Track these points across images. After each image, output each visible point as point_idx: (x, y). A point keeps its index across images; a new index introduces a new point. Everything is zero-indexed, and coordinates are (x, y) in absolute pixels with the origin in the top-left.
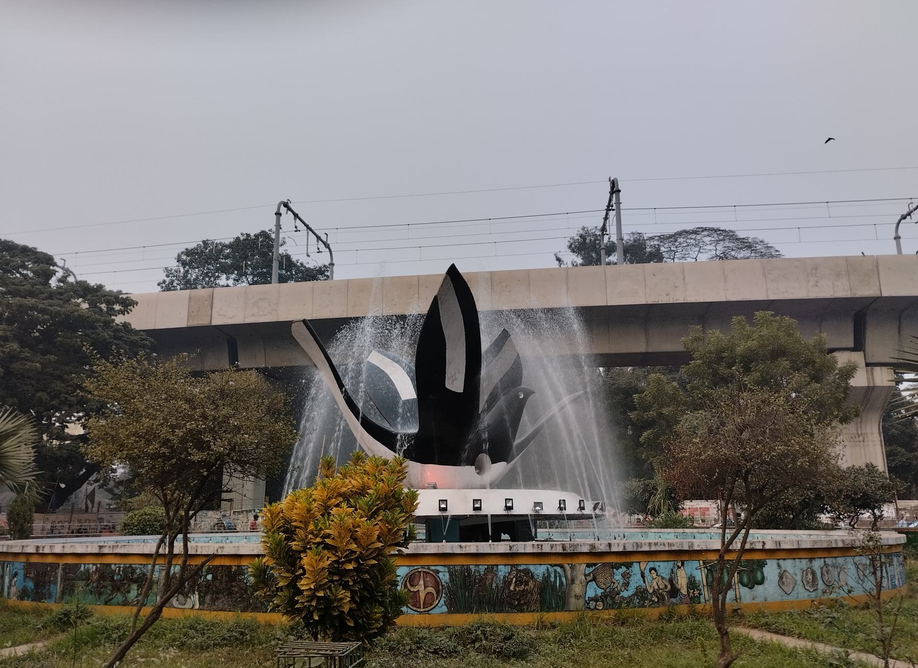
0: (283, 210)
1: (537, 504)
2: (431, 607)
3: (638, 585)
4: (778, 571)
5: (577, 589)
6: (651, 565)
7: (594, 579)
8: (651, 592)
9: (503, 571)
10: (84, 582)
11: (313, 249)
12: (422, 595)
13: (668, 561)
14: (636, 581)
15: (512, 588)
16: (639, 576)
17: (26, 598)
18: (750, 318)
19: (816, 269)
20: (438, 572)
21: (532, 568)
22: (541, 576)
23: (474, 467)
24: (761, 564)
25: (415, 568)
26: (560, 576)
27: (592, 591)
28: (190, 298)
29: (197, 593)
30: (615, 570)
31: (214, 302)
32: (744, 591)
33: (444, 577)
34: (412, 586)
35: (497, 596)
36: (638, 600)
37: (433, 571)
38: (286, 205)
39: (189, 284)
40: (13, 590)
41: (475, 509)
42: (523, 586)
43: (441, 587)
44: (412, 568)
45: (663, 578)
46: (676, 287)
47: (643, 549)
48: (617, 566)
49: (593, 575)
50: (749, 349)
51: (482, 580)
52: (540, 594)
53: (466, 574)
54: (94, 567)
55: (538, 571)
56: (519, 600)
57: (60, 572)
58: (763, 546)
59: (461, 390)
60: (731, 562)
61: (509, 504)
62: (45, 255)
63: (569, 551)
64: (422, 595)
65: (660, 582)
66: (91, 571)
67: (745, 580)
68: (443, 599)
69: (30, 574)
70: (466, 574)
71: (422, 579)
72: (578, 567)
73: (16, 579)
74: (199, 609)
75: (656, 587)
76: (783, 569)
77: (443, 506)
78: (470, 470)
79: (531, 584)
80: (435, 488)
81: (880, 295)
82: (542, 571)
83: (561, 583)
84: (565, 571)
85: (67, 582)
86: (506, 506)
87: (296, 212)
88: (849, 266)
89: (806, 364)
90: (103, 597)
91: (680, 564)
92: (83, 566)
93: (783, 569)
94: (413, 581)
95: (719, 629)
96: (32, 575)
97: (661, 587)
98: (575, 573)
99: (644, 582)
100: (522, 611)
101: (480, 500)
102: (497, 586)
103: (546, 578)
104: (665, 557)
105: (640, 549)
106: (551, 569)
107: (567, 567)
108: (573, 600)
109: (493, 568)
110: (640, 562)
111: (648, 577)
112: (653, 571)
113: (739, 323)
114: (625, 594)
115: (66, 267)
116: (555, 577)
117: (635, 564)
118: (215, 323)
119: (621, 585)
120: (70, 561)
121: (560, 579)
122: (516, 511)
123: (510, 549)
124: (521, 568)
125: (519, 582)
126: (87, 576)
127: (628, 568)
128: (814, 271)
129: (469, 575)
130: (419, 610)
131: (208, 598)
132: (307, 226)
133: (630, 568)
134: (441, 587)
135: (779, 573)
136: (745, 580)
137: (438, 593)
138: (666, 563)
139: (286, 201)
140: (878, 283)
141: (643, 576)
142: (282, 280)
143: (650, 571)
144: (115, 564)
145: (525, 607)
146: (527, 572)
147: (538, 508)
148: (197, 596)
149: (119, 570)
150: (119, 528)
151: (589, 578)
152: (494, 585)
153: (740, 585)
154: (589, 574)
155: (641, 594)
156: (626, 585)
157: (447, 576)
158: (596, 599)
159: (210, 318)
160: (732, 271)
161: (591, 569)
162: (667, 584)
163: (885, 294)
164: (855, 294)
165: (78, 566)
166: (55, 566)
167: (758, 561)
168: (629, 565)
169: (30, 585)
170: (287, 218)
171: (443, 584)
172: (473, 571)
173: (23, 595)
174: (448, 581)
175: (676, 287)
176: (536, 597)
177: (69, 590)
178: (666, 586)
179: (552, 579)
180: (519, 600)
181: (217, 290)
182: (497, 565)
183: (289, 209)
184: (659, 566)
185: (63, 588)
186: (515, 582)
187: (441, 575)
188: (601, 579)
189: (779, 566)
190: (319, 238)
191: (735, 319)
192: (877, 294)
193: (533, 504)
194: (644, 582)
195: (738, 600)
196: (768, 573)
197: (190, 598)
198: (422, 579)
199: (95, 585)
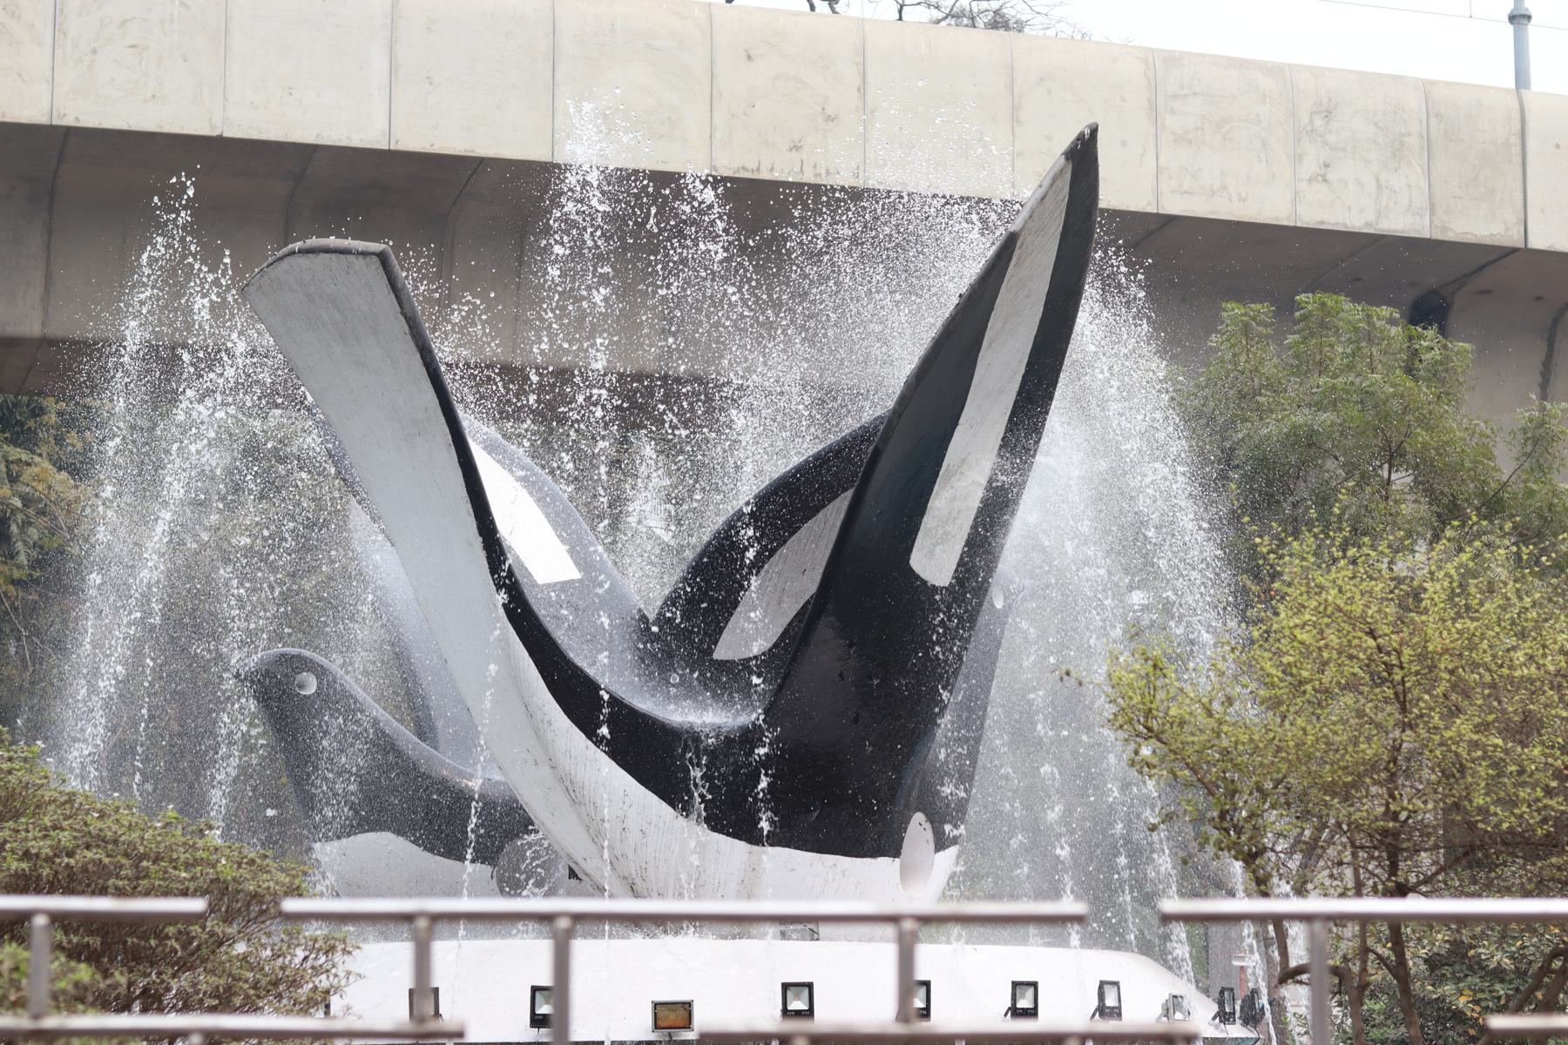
19: (1328, 115)
46: (830, 119)
77: (1024, 1003)
81: (1521, 245)
88: (1433, 121)
122: (1049, 1020)
128: (1319, 123)
140: (1520, 196)
150: (90, 999)
163: (1536, 242)
164: (1445, 229)
175: (830, 119)
191: (1233, 310)
192: (1512, 238)
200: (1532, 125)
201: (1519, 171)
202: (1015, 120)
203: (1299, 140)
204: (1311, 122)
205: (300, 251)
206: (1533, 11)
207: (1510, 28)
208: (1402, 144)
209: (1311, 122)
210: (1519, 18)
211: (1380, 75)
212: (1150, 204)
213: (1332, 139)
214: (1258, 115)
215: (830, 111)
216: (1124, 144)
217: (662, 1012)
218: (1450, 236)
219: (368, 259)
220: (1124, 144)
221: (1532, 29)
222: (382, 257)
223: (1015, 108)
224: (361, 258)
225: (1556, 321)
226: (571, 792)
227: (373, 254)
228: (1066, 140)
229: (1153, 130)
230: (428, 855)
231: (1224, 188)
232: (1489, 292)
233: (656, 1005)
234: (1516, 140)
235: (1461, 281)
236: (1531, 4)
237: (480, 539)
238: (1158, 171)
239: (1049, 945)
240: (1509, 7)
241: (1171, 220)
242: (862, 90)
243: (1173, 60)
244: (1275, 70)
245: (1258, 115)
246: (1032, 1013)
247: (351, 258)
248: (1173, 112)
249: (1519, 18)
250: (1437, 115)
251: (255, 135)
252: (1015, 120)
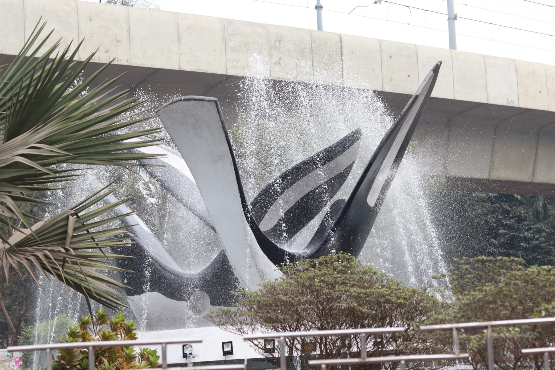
19: (280, 41)
77: (227, 349)
88: (313, 44)
128: (277, 44)
164: (143, 64)
175: (118, 41)
203: (271, 50)
204: (275, 44)
205: (184, 100)
206: (323, 5)
207: (315, 11)
208: (304, 52)
209: (275, 44)
210: (318, 8)
211: (296, 28)
212: (224, 71)
214: (258, 41)
215: (118, 39)
216: (215, 51)
219: (211, 103)
220: (215, 51)
221: (323, 11)
222: (215, 102)
223: (179, 39)
224: (208, 103)
226: (262, 276)
227: (213, 101)
229: (224, 46)
230: (168, 299)
234: (339, 50)
236: (322, 3)
237: (239, 194)
239: (198, 327)
240: (315, 4)
242: (129, 31)
243: (230, 22)
244: (263, 26)
245: (258, 41)
246: (231, 353)
247: (204, 102)
248: (231, 40)
249: (318, 8)
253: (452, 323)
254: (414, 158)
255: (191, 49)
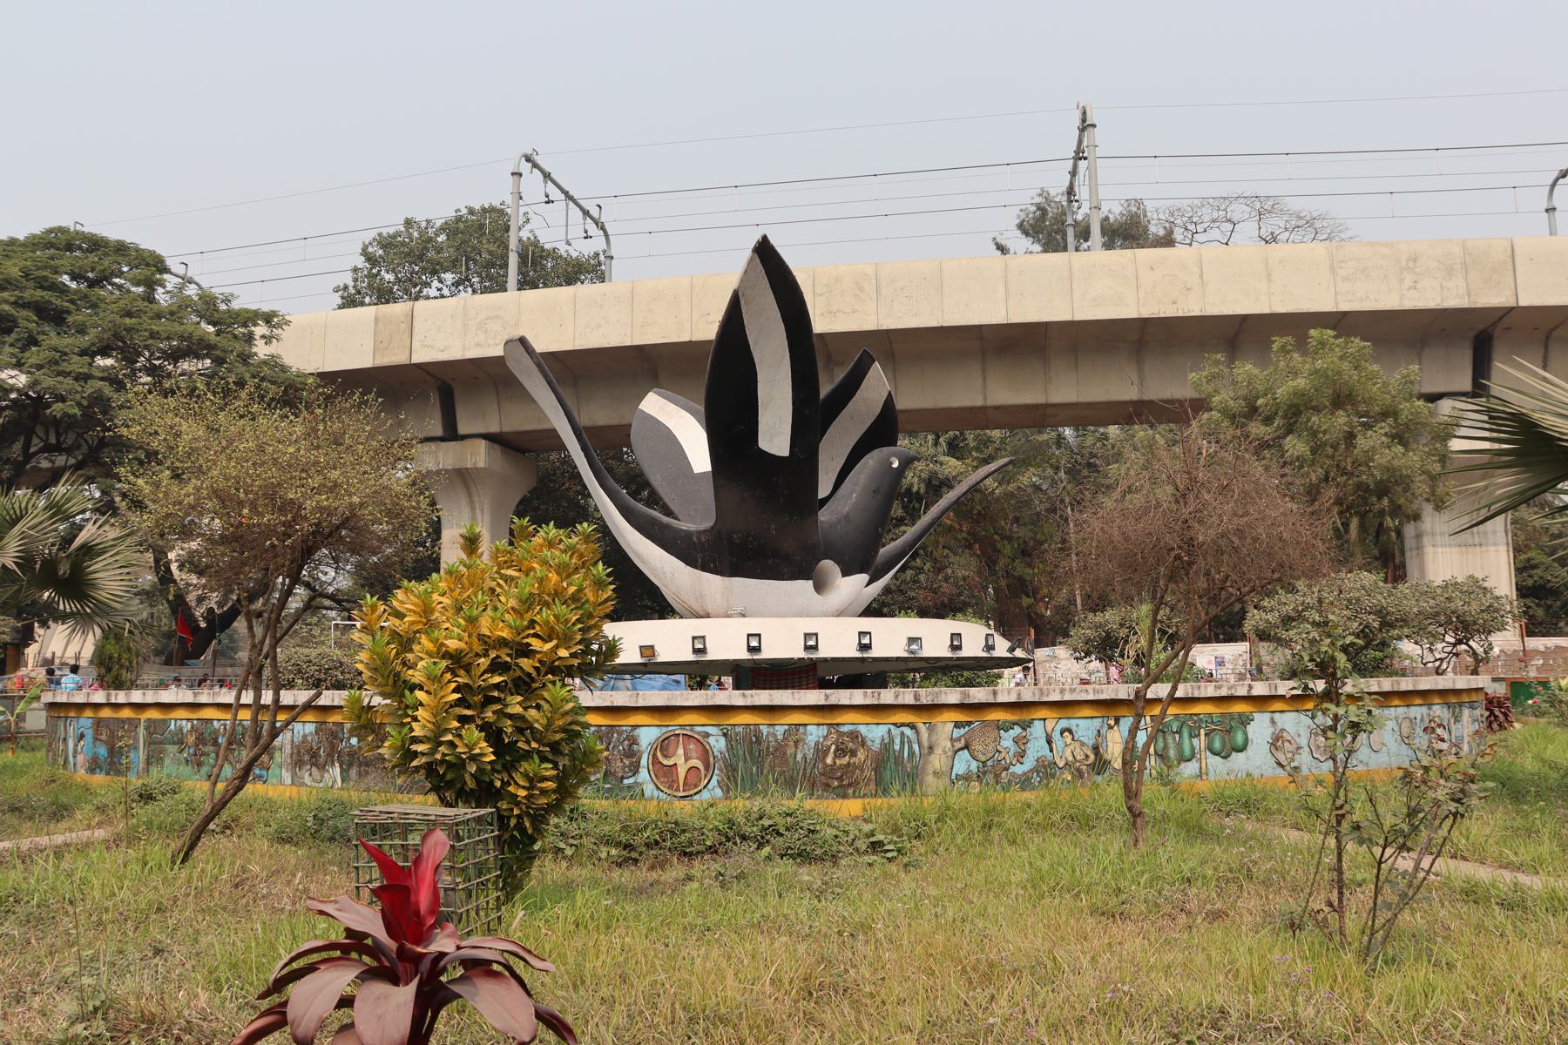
0: (525, 167)
1: (912, 640)
2: (696, 790)
3: (1039, 755)
4: (1272, 730)
5: (937, 761)
6: (1064, 723)
7: (967, 747)
8: (1061, 765)
9: (815, 733)
10: (176, 747)
11: (576, 232)
12: (682, 771)
13: (1092, 718)
14: (1037, 748)
15: (829, 761)
16: (1043, 742)
17: (98, 770)
18: (1302, 344)
19: (1415, 260)
20: (707, 735)
21: (863, 729)
22: (878, 741)
23: (811, 582)
24: (1245, 721)
25: (670, 728)
26: (910, 742)
27: (963, 763)
28: (377, 319)
29: (337, 765)
30: (1002, 732)
31: (415, 324)
32: (1214, 762)
33: (718, 744)
34: (666, 756)
35: (804, 774)
36: (1038, 779)
37: (698, 733)
38: (528, 159)
39: (385, 296)
40: (80, 758)
41: (807, 648)
42: (847, 757)
43: (711, 759)
44: (665, 729)
45: (1083, 744)
47: (1051, 699)
48: (1007, 727)
49: (966, 741)
50: (1297, 393)
51: (780, 748)
52: (876, 770)
53: (754, 739)
54: (189, 724)
55: (874, 734)
56: (840, 779)
57: (142, 732)
58: (1249, 691)
59: (787, 455)
60: (1195, 718)
61: (866, 641)
62: (152, 254)
63: (925, 702)
64: (682, 771)
65: (1078, 750)
66: (185, 731)
67: (1217, 745)
68: (715, 778)
69: (101, 734)
70: (754, 739)
71: (681, 746)
72: (940, 727)
73: (82, 743)
74: (342, 789)
75: (1070, 758)
76: (1280, 726)
77: (754, 643)
78: (807, 586)
79: (861, 755)
80: (744, 616)
82: (880, 734)
83: (911, 753)
84: (917, 733)
85: (153, 747)
86: (860, 643)
87: (548, 169)
88: (1467, 256)
89: (1384, 415)
90: (205, 770)
91: (1112, 722)
92: (173, 722)
93: (1280, 726)
94: (666, 750)
95: (1130, 809)
96: (104, 737)
97: (1078, 758)
98: (934, 738)
99: (1051, 751)
100: (845, 796)
101: (816, 635)
102: (805, 758)
103: (887, 746)
104: (1087, 712)
105: (1045, 699)
106: (896, 732)
107: (923, 729)
108: (930, 779)
109: (798, 730)
110: (1045, 720)
111: (1058, 742)
112: (1066, 734)
113: (1283, 349)
114: (1018, 769)
115: (189, 275)
116: (902, 743)
117: (1036, 723)
118: (416, 359)
119: (1011, 754)
120: (154, 714)
121: (910, 748)
122: (877, 652)
123: (826, 700)
124: (845, 729)
125: (841, 751)
126: (179, 740)
127: (1024, 729)
128: (1411, 264)
129: (758, 741)
130: (676, 794)
131: (353, 772)
132: (566, 193)
133: (1028, 729)
134: (711, 759)
135: (1273, 733)
136: (1217, 745)
137: (707, 768)
138: (1090, 720)
139: (529, 152)
140: (1513, 285)
141: (1049, 742)
142: (526, 283)
143: (1062, 734)
144: (219, 720)
145: (850, 791)
146: (854, 735)
147: (914, 647)
148: (338, 770)
149: (225, 729)
151: (958, 745)
152: (799, 757)
153: (1208, 753)
154: (959, 739)
155: (1046, 770)
156: (1021, 755)
157: (722, 741)
158: (966, 778)
159: (408, 351)
160: (1280, 262)
161: (962, 731)
162: (1089, 753)
163: (1523, 303)
164: (1476, 303)
165: (165, 722)
166: (134, 724)
167: (1240, 715)
168: (1026, 725)
169: (103, 751)
170: (533, 180)
171: (716, 753)
172: (765, 734)
173: (94, 766)
174: (723, 748)
176: (869, 773)
177: (154, 758)
178: (1087, 756)
179: (897, 747)
180: (840, 779)
181: (421, 304)
182: (805, 725)
183: (535, 165)
184: (1077, 725)
185: (148, 755)
186: (835, 752)
187: (712, 740)
188: (977, 747)
189: (1273, 722)
190: (586, 213)
192: (1511, 303)
193: (906, 641)
194: (1051, 751)
195: (1204, 777)
196: (1254, 732)
197: (328, 771)
198: (681, 746)
199: (192, 750)
200: (1517, 253)
201: (1512, 273)
202: (1269, 280)
206: (1556, 206)
213: (1418, 270)
215: (1188, 286)
217: (644, 650)
218: (1479, 306)
220: (1320, 284)
225: (1548, 338)
228: (752, 244)
231: (1367, 297)
232: (1508, 329)
233: (641, 647)
234: (1509, 260)
235: (1494, 324)
238: (1336, 294)
241: (1345, 313)
242: (1201, 276)
250: (1469, 254)
251: (955, 324)
252: (1269, 280)
253: (1516, 576)
254: (1346, 383)
255: (1286, 286)
